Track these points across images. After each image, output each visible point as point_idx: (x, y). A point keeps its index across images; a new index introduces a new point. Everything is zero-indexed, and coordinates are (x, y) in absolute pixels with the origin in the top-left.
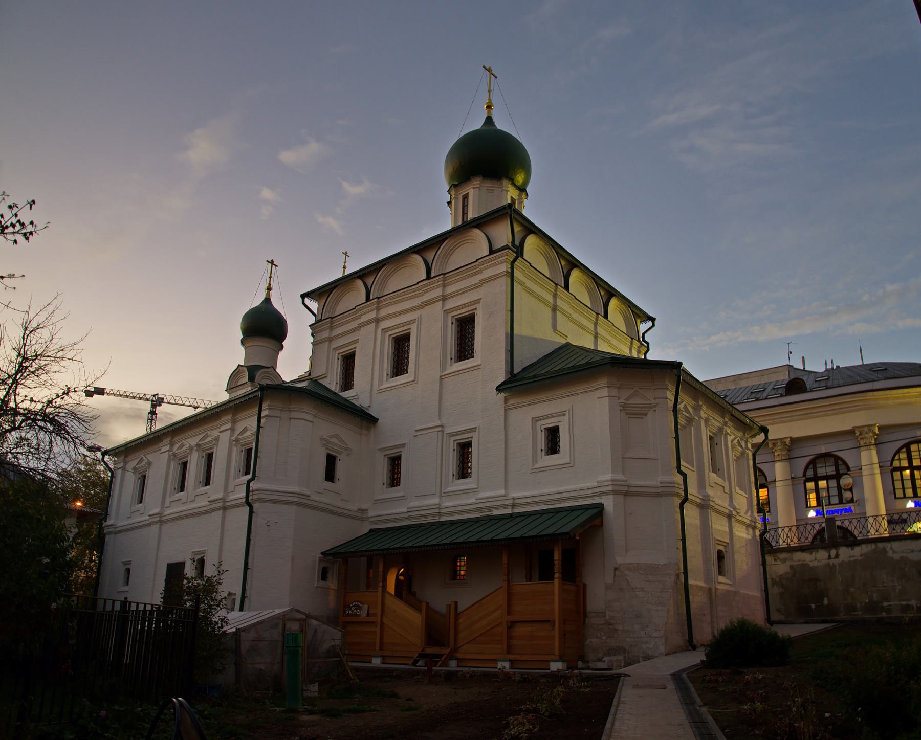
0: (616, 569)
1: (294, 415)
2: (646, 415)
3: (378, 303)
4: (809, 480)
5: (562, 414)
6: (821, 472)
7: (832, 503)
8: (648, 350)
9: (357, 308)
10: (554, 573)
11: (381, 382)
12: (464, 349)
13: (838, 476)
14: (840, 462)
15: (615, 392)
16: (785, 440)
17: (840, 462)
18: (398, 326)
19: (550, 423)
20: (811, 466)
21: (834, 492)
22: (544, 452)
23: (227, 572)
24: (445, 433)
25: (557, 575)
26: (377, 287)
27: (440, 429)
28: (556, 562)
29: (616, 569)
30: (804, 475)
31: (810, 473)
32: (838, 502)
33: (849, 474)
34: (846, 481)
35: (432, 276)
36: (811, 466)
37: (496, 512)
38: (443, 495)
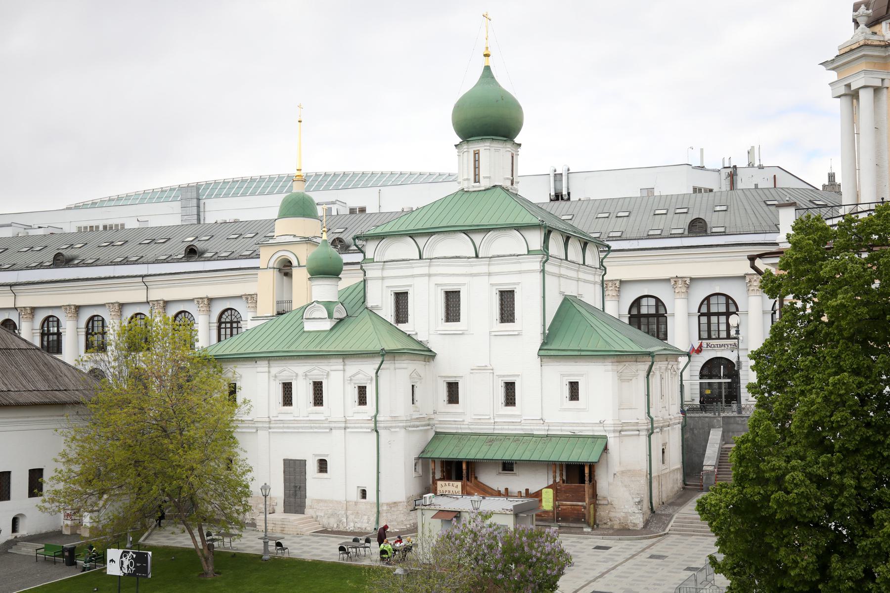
0: (615, 474)
1: (397, 365)
3: (430, 262)
4: (703, 315)
5: (582, 375)
6: (714, 309)
7: (721, 337)
8: (605, 274)
12: (507, 313)
13: (728, 314)
14: (730, 301)
15: (615, 368)
16: (686, 279)
17: (730, 301)
20: (706, 302)
21: (723, 327)
23: (441, 498)
24: (495, 374)
25: (586, 482)
26: (428, 249)
28: (586, 475)
29: (615, 474)
30: (699, 311)
31: (704, 310)
32: (726, 337)
33: (737, 314)
34: (733, 320)
36: (706, 302)
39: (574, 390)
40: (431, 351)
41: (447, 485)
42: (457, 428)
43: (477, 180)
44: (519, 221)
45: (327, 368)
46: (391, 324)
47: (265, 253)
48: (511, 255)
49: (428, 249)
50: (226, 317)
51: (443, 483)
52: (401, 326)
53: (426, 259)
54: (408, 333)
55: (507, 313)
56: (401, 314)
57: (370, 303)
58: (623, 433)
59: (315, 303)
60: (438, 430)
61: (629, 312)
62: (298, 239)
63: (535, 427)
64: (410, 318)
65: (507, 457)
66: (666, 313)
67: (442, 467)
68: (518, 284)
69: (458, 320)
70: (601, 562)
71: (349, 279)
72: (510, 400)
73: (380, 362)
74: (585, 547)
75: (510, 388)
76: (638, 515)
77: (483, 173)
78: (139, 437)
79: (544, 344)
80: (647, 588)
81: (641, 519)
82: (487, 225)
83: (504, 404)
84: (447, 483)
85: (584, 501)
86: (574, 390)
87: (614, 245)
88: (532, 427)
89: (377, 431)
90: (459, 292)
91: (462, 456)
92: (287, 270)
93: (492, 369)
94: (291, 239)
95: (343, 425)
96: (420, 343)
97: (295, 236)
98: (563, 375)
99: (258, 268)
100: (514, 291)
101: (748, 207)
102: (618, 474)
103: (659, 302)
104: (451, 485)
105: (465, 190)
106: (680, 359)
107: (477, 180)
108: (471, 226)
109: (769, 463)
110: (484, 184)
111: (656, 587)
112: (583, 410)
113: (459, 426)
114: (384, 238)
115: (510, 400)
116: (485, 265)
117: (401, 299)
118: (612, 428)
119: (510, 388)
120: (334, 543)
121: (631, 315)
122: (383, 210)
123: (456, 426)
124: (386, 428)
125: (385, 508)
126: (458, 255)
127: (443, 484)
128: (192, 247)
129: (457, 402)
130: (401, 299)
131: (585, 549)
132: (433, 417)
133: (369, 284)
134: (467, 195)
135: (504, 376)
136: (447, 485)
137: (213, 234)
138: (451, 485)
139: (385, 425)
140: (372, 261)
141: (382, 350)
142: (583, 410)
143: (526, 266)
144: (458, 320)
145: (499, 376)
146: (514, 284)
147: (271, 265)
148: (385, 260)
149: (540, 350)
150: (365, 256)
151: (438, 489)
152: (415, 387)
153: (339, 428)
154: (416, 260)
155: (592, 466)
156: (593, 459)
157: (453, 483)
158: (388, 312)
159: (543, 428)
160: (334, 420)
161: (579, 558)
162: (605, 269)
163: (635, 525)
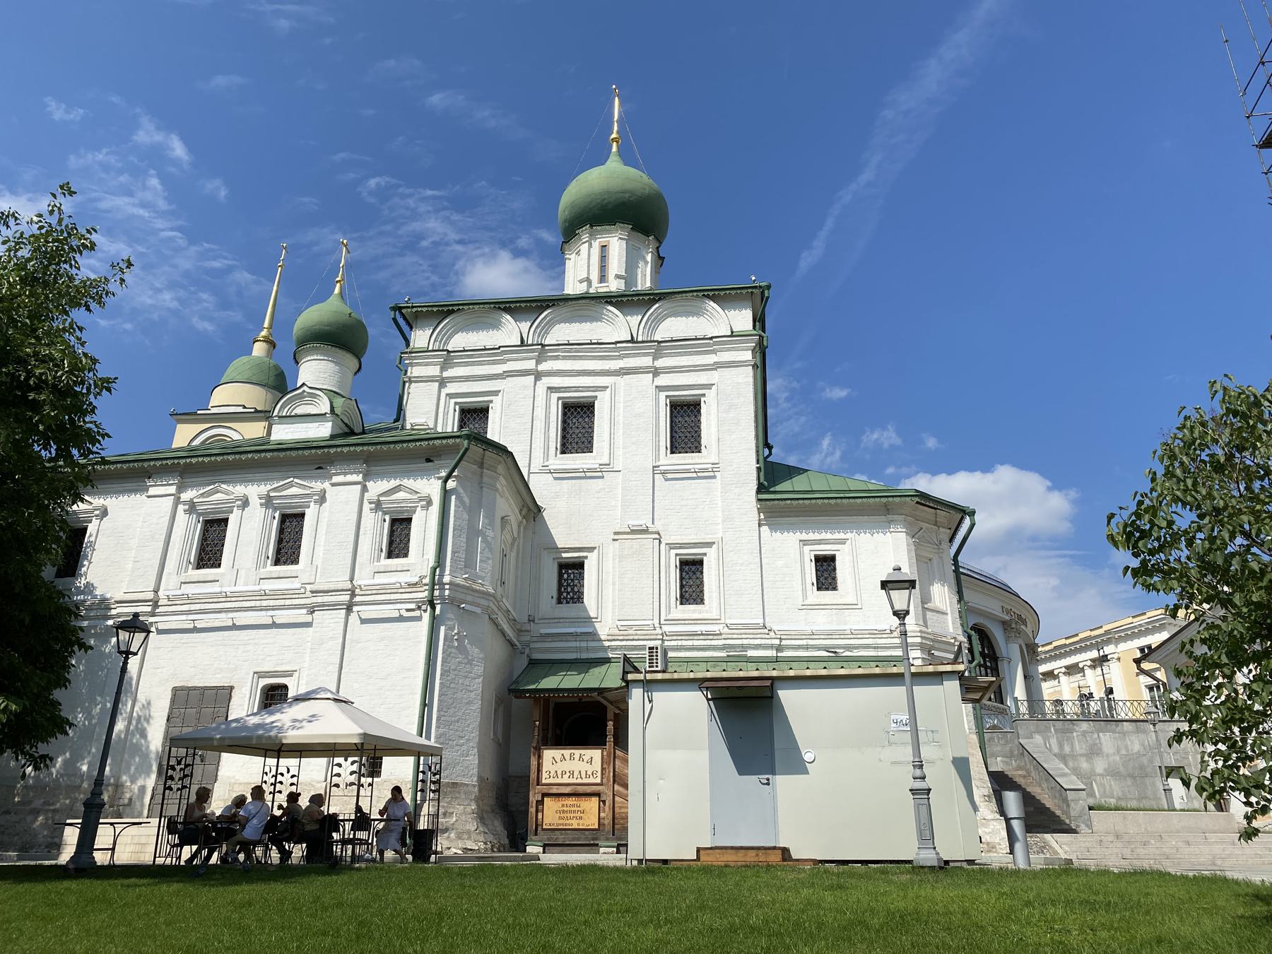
9: (501, 349)
10: (607, 736)
11: (546, 456)
18: (577, 389)
19: (825, 550)
22: (269, 562)
25: (610, 738)
37: (751, 653)
38: (662, 622)
39: (826, 570)
41: (567, 757)
42: (579, 650)
45: (317, 485)
60: (536, 656)
63: (752, 642)
69: (697, 448)
75: (691, 569)
78: (336, 935)
84: (567, 752)
86: (826, 570)
88: (745, 642)
95: (345, 598)
98: (805, 542)
104: (577, 757)
109: (1063, 758)
113: (584, 644)
114: (548, 307)
118: (919, 640)
119: (691, 569)
120: (92, 539)
123: (578, 644)
125: (755, 551)
127: (558, 757)
132: (527, 627)
135: (682, 546)
136: (567, 757)
138: (577, 757)
144: (697, 448)
145: (672, 546)
153: (333, 606)
157: (583, 752)
159: (769, 642)
160: (326, 587)
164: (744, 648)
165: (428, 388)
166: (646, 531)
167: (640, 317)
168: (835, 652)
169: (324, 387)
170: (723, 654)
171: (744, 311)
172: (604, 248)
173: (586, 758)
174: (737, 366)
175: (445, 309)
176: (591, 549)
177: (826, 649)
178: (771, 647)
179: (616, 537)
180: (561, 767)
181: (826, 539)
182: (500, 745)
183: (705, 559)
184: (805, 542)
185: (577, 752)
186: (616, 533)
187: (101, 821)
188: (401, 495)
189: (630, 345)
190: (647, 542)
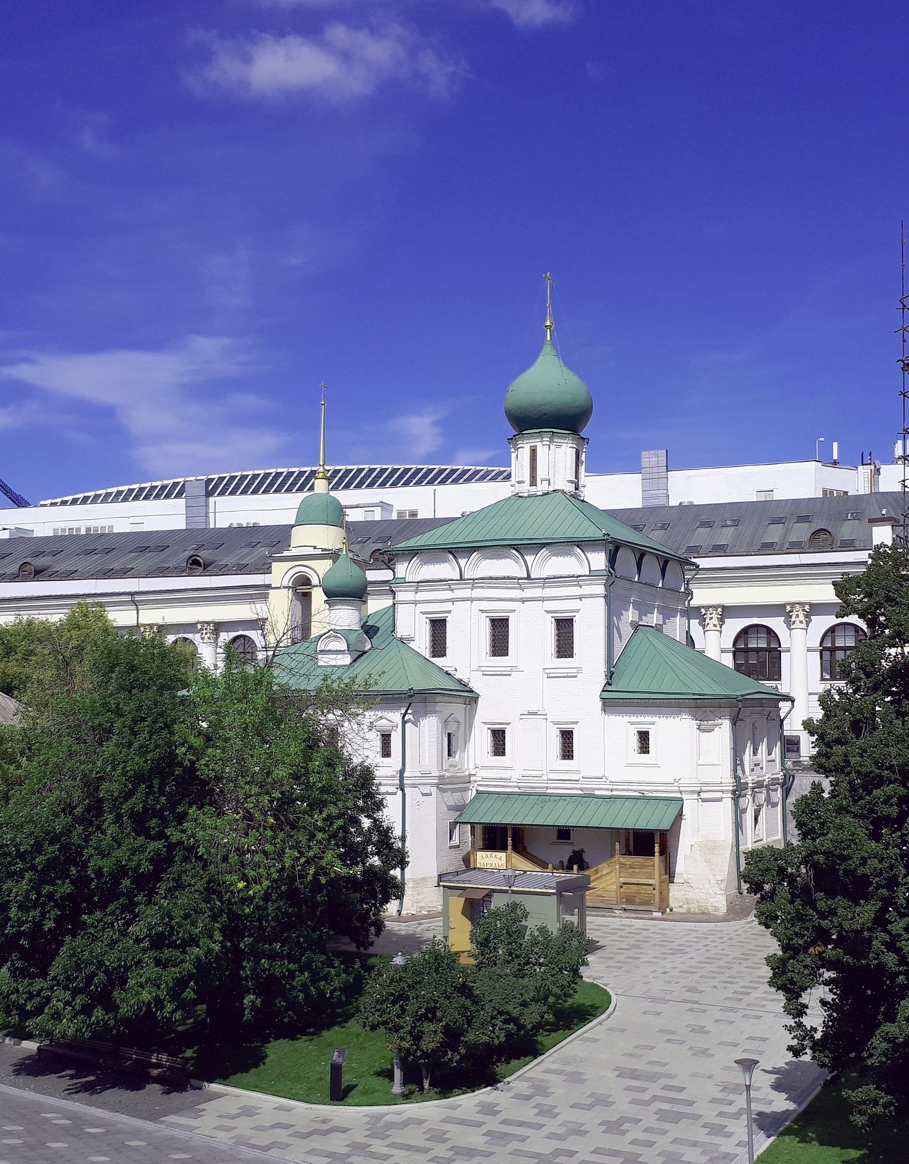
0: (692, 845)
2: (713, 730)
12: (565, 648)
19: (643, 728)
20: (829, 634)
22: (488, 655)
25: (657, 854)
27: (544, 717)
29: (692, 845)
35: (588, 555)
37: (597, 793)
39: (644, 737)
40: (472, 691)
41: (489, 856)
43: (533, 483)
44: (580, 534)
46: (425, 658)
47: (278, 568)
48: (504, 578)
49: (471, 566)
50: (239, 646)
51: (483, 854)
52: (437, 661)
53: (468, 580)
54: (446, 669)
55: (565, 648)
56: (439, 647)
57: (400, 632)
58: (703, 795)
59: (331, 632)
61: (734, 645)
62: (319, 552)
64: (448, 651)
65: (561, 822)
66: (780, 647)
67: (484, 834)
68: (578, 611)
69: (571, 655)
70: (624, 949)
71: (375, 605)
72: (567, 753)
73: (407, 706)
74: (652, 935)
75: (567, 736)
76: (721, 896)
77: (541, 474)
79: (608, 684)
80: (715, 987)
81: (725, 902)
82: (540, 539)
83: (560, 757)
84: (489, 853)
85: (654, 879)
86: (644, 737)
87: (703, 563)
89: (402, 790)
90: (508, 619)
91: (507, 820)
92: (304, 589)
93: (546, 715)
94: (311, 551)
96: (460, 681)
97: (315, 548)
99: (269, 587)
100: (446, 620)
101: (176, 541)
102: (696, 846)
103: (770, 633)
104: (494, 856)
105: (520, 495)
106: (781, 704)
107: (533, 483)
108: (522, 539)
110: (542, 487)
111: (726, 985)
112: (655, 765)
114: (475, 551)
115: (567, 753)
116: (539, 587)
117: (438, 626)
119: (567, 736)
121: (736, 649)
122: (217, 527)
124: (414, 786)
126: (510, 575)
128: (198, 558)
129: (503, 754)
130: (438, 626)
131: (650, 937)
133: (399, 608)
134: (522, 500)
136: (489, 856)
137: (97, 548)
138: (494, 856)
139: (413, 782)
140: (403, 581)
141: (410, 689)
142: (655, 765)
143: (587, 590)
144: (571, 655)
145: (555, 723)
146: (572, 611)
147: (285, 583)
148: (419, 580)
149: (603, 691)
150: (394, 575)
151: (478, 862)
152: (453, 739)
154: (401, 591)
155: (663, 834)
156: (665, 825)
158: (422, 643)
161: (641, 949)
162: (692, 592)
163: (716, 909)
164: (594, 789)
165: (409, 608)
166: (535, 714)
167: (466, 560)
168: (643, 794)
169: (257, 1116)
170: (580, 792)
171: (600, 553)
172: (533, 451)
173: (498, 857)
174: (561, 597)
175: (413, 552)
176: (509, 724)
177: (638, 791)
178: (608, 789)
179: (522, 717)
180: (486, 861)
181: (644, 721)
182: (188, 1141)
183: (574, 619)
184: (632, 723)
185: (494, 854)
186: (521, 715)
187: (368, 589)
188: (384, 722)
189: (526, 581)
190: (537, 721)
